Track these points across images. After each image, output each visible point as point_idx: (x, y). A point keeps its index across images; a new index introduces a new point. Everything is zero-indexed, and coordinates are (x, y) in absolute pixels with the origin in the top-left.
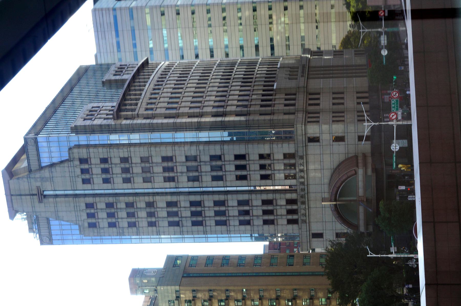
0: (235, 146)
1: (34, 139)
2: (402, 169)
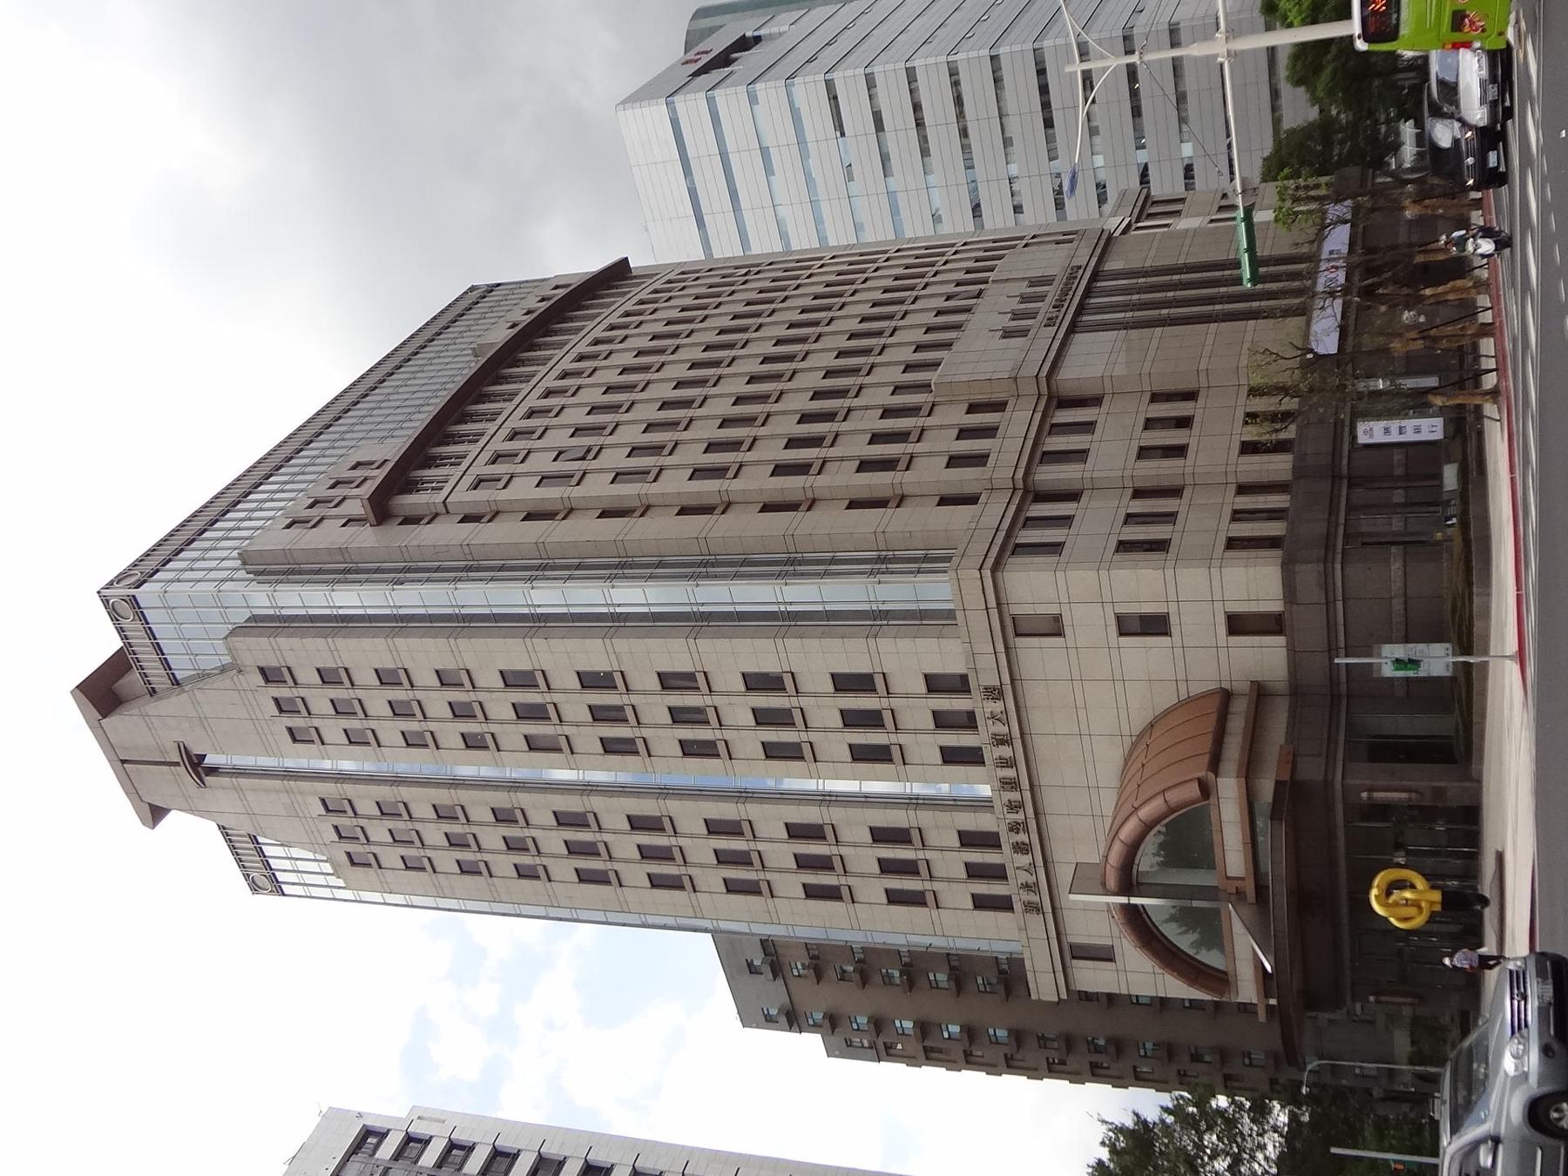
1: (127, 598)
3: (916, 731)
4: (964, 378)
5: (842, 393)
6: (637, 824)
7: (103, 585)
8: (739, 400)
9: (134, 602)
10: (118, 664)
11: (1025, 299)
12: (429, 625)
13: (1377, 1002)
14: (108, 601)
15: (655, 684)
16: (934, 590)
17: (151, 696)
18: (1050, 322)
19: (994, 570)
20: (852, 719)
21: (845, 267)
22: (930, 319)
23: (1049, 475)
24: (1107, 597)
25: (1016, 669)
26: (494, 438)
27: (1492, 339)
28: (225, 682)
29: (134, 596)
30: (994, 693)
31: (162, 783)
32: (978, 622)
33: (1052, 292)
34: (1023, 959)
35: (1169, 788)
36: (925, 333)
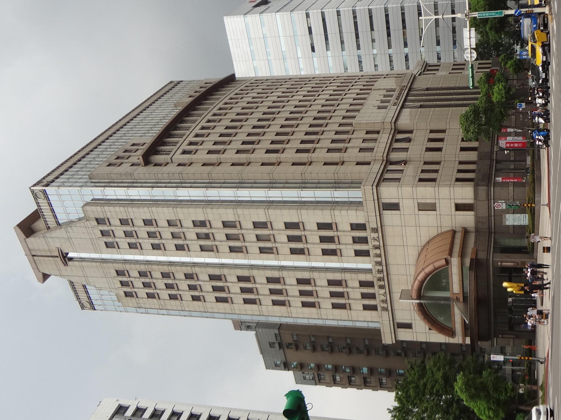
0: (283, 211)
1: (42, 191)
2: (509, 290)
3: (346, 244)
4: (365, 122)
5: (320, 125)
6: (241, 279)
7: (31, 186)
8: (249, 135)
9: (44, 192)
10: (36, 216)
11: (385, 96)
12: (165, 203)
13: (502, 337)
14: (33, 192)
15: (251, 226)
16: (354, 194)
17: (48, 229)
18: (395, 104)
19: (377, 186)
20: (323, 240)
21: (318, 82)
22: (351, 101)
23: (395, 156)
24: (415, 197)
25: (382, 222)
26: (189, 136)
28: (82, 224)
29: (45, 190)
30: (375, 230)
31: (47, 266)
32: (371, 206)
33: (395, 94)
34: (380, 329)
35: (435, 262)
36: (318, 113)
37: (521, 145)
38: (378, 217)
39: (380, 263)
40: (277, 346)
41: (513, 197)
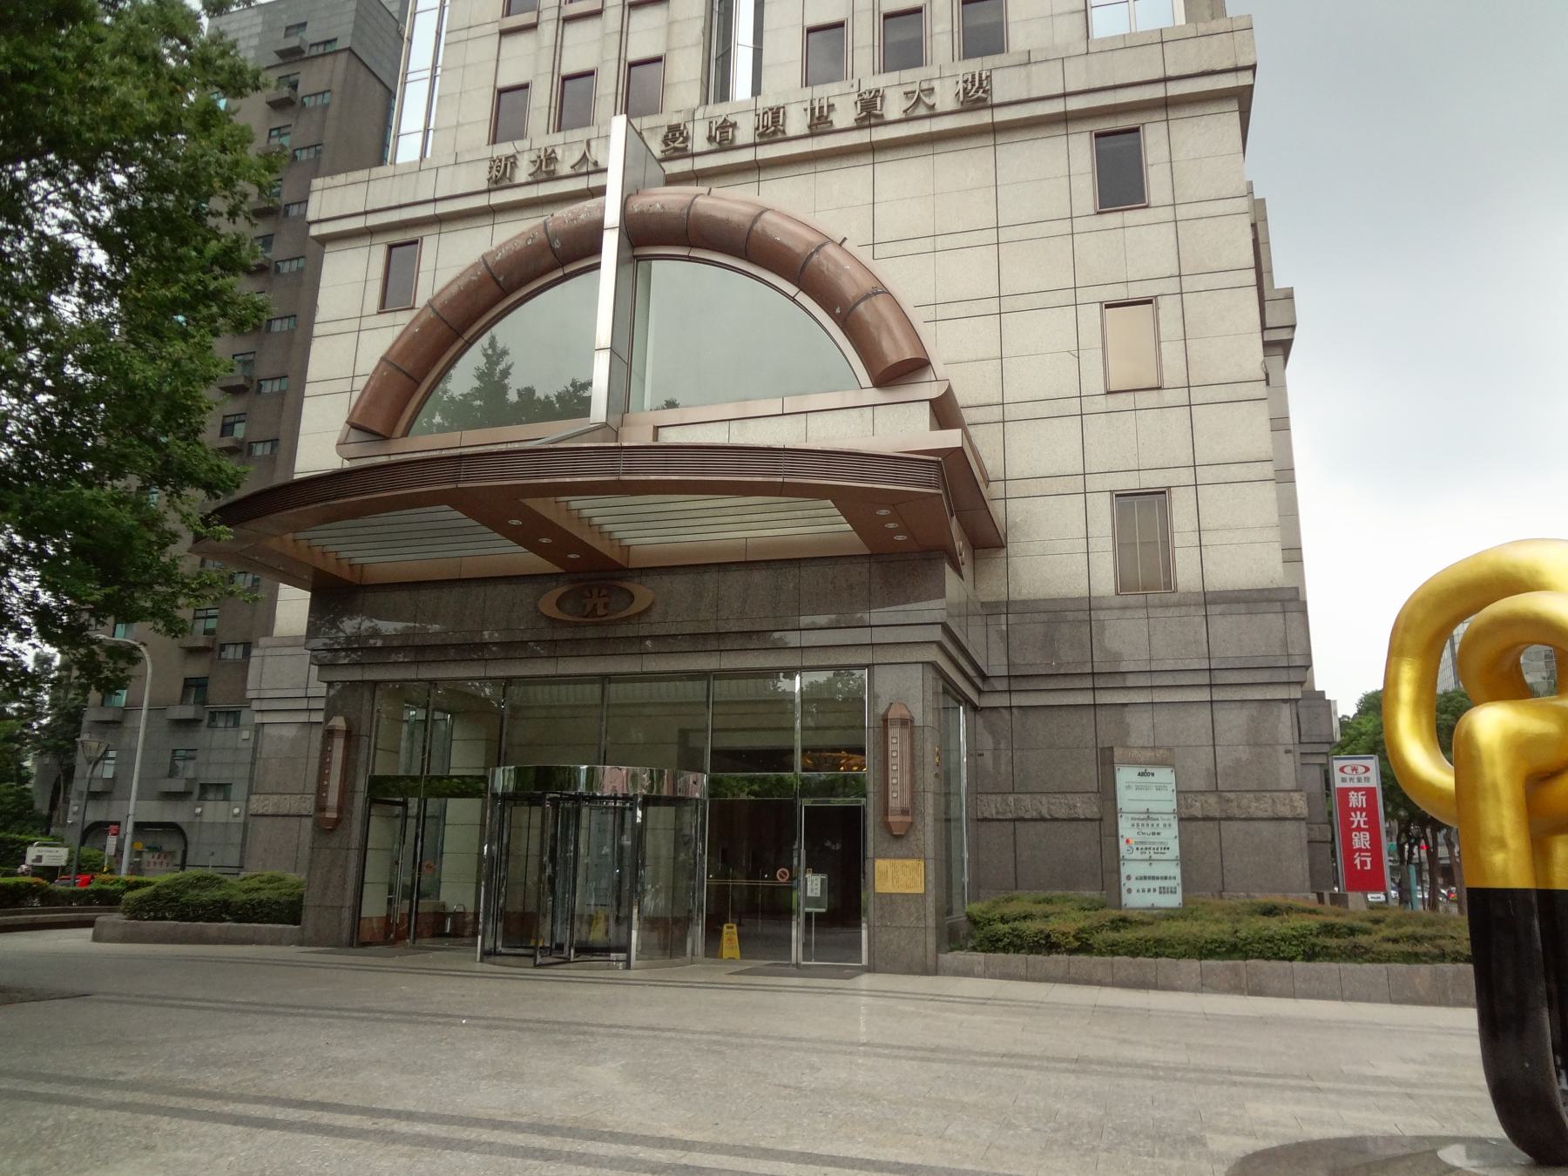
27: (809, 894)
37: (1363, 863)
38: (1056, 107)
39: (772, 127)
40: (293, 42)
41: (1237, 812)
